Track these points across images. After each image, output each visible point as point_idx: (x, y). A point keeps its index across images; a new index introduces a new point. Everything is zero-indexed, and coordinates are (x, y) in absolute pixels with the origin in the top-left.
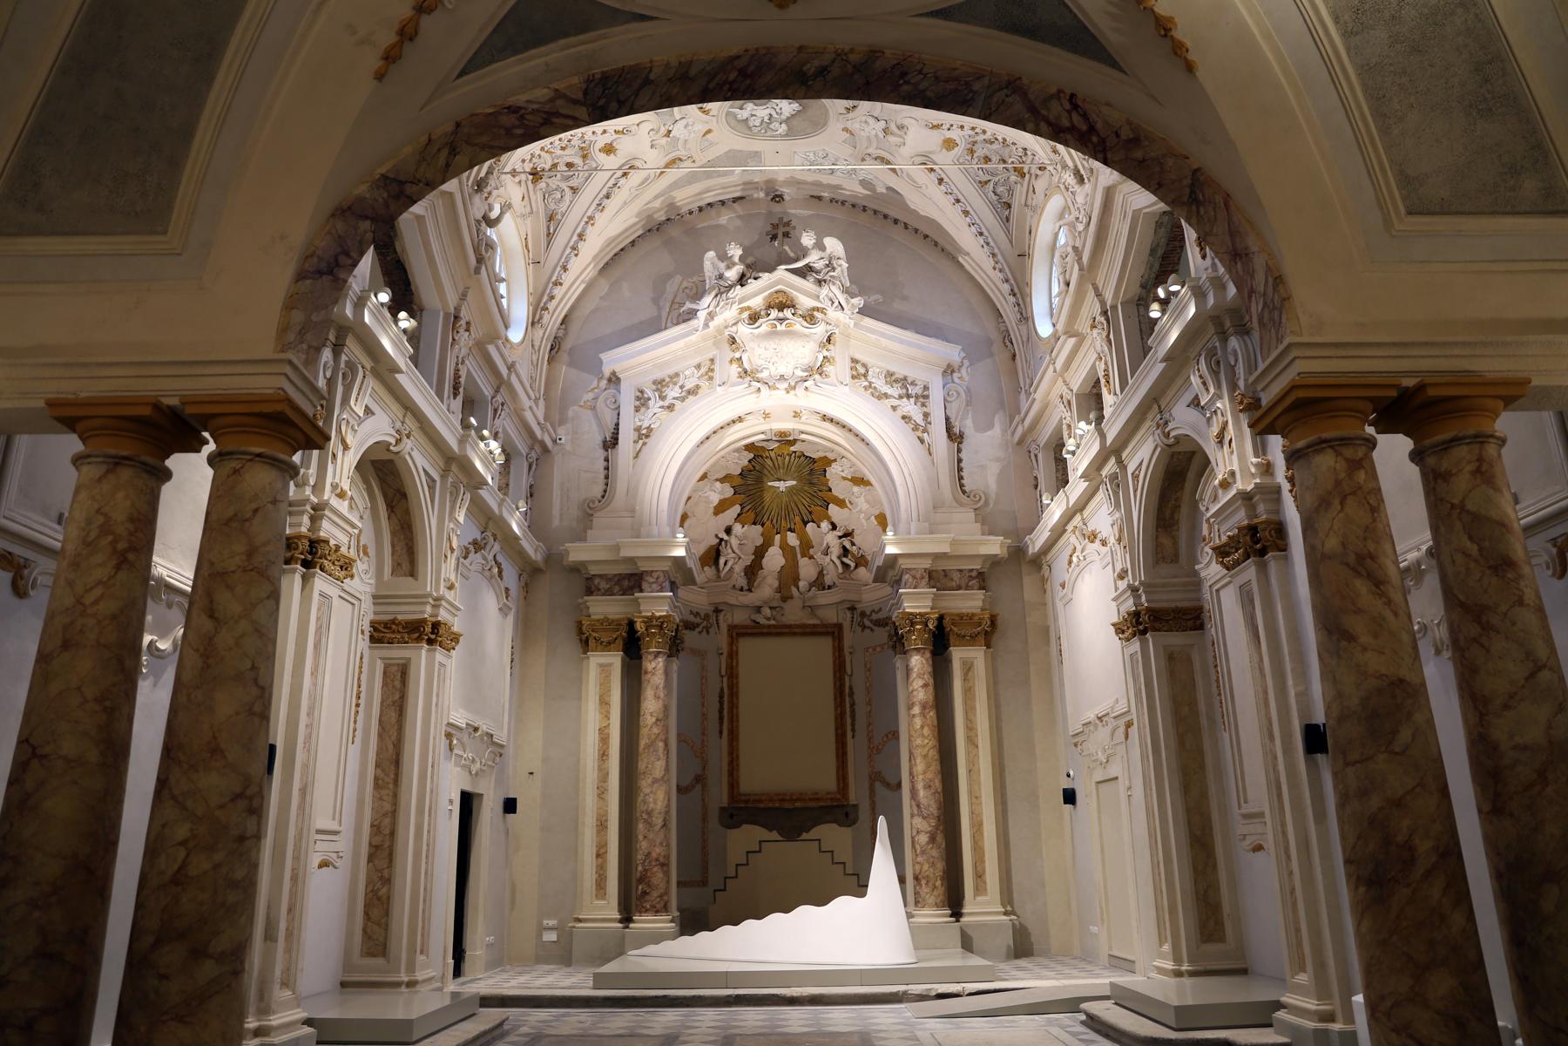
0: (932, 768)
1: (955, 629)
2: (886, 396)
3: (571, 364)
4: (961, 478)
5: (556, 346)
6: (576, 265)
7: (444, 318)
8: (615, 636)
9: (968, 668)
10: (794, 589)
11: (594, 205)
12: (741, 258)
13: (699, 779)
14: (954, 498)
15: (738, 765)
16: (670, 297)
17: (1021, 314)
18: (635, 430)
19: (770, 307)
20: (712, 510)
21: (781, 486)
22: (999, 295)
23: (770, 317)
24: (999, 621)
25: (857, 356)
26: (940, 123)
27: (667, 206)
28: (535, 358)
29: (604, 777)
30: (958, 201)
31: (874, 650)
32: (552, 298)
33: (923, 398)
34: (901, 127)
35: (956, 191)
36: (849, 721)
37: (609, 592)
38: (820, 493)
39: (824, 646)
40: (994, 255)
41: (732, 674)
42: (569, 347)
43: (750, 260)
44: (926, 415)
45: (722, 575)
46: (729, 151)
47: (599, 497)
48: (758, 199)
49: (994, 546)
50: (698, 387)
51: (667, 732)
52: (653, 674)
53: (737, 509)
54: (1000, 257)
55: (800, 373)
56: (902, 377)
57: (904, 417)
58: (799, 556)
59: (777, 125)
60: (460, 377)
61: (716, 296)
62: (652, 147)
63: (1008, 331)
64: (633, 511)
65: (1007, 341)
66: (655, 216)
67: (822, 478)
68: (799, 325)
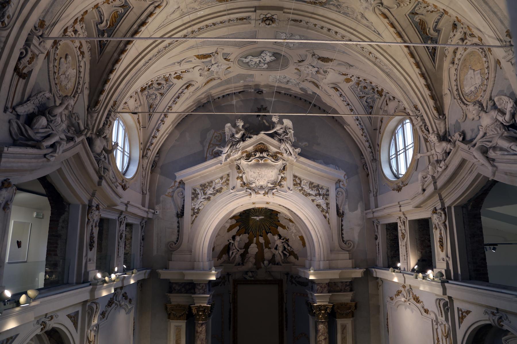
1: (339, 311)
2: (310, 195)
4: (342, 234)
5: (154, 165)
6: (163, 128)
7: (82, 208)
8: (182, 313)
9: (344, 328)
10: (262, 264)
11: (172, 102)
12: (243, 126)
14: (339, 244)
17: (373, 157)
18: (191, 209)
19: (256, 151)
20: (227, 230)
21: (258, 218)
22: (363, 146)
23: (257, 156)
25: (297, 174)
26: (347, 73)
28: (144, 173)
30: (348, 104)
32: (152, 144)
33: (326, 196)
34: (325, 72)
35: (348, 100)
36: (285, 323)
37: (180, 292)
40: (363, 129)
41: (235, 301)
44: (327, 204)
45: (231, 259)
46: (238, 74)
47: (175, 241)
48: (251, 92)
49: (358, 273)
50: (221, 188)
52: (201, 334)
53: (238, 228)
54: (365, 130)
55: (270, 185)
57: (317, 205)
58: (264, 247)
60: (94, 238)
61: (231, 147)
62: (200, 76)
64: (191, 251)
65: (365, 167)
66: (202, 101)
68: (269, 161)
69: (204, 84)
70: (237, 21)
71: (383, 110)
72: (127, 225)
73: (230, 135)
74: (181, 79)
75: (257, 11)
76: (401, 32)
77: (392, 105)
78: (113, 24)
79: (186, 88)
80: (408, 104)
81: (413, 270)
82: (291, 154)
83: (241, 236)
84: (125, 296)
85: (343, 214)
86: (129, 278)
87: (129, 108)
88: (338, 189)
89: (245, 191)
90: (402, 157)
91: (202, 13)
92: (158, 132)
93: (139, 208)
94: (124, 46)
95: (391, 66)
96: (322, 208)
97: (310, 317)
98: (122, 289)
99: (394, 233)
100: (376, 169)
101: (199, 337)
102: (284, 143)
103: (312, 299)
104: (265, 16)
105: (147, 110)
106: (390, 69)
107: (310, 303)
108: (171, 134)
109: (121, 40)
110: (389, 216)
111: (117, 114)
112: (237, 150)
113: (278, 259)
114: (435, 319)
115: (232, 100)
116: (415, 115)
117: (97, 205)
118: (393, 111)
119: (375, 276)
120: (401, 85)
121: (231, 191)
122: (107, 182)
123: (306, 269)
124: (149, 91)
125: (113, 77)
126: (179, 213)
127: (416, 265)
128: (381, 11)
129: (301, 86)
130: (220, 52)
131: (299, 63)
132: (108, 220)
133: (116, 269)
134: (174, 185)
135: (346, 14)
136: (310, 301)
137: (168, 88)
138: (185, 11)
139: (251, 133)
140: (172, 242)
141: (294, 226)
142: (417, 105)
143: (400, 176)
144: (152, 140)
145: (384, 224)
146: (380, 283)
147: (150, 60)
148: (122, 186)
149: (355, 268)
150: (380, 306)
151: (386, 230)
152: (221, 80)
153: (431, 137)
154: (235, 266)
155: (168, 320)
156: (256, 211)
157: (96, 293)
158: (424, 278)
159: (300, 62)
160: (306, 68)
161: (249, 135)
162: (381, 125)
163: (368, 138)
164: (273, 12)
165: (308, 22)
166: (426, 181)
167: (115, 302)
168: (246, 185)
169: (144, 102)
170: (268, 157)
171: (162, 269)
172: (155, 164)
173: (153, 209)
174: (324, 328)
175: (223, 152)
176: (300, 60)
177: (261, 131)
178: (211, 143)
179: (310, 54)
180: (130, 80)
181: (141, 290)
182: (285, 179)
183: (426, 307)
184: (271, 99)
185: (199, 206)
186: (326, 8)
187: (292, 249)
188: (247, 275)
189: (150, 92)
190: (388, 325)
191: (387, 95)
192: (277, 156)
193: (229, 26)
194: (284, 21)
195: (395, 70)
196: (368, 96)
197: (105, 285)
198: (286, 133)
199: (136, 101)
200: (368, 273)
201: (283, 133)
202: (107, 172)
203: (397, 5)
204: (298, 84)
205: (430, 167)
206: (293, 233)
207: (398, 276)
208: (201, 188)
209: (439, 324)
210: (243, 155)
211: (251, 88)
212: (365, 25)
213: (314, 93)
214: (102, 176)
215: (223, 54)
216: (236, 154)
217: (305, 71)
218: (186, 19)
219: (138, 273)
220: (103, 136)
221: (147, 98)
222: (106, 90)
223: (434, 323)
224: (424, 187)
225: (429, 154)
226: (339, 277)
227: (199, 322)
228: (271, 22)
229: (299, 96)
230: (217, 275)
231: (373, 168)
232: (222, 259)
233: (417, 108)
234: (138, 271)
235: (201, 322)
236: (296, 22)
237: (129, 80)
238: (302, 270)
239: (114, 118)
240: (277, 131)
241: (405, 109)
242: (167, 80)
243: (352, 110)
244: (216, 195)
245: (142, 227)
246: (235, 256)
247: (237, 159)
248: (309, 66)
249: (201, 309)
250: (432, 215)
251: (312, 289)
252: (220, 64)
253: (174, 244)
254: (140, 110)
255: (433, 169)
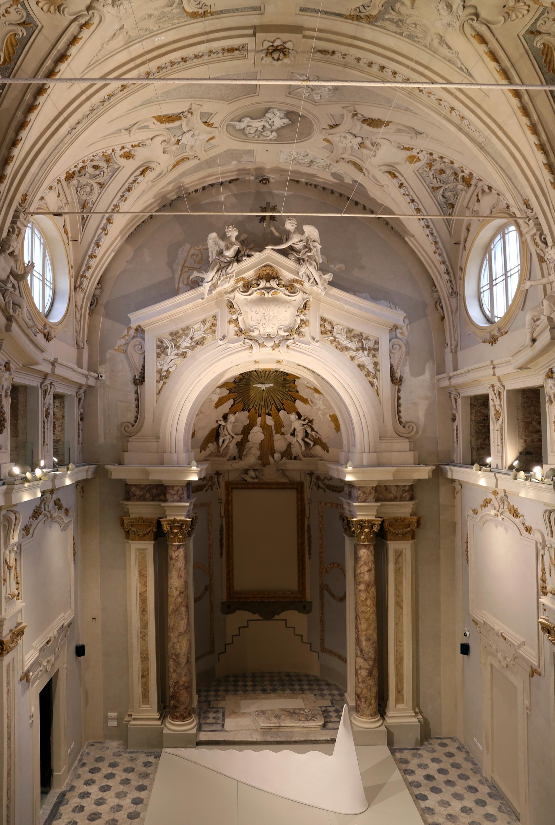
0: (372, 627)
1: (392, 530)
3: (107, 316)
4: (399, 412)
5: (94, 302)
6: (106, 242)
9: (399, 554)
10: (271, 459)
12: (237, 238)
13: (208, 588)
15: (233, 574)
16: (182, 263)
17: (452, 289)
19: (259, 278)
21: (263, 387)
23: (260, 286)
24: (422, 522)
25: (326, 316)
26: (411, 147)
27: (178, 188)
28: (78, 316)
29: (144, 625)
30: (413, 201)
31: (326, 504)
32: (89, 268)
33: (374, 351)
35: (412, 193)
36: (307, 548)
37: (142, 498)
38: (290, 393)
39: (291, 496)
40: (436, 243)
41: (228, 515)
42: (105, 302)
43: (244, 237)
44: (376, 364)
45: (221, 450)
46: (228, 150)
47: (132, 421)
48: (249, 181)
50: (204, 338)
51: (188, 599)
52: (177, 560)
53: (231, 402)
54: (440, 244)
55: (282, 333)
56: (359, 333)
57: (359, 366)
58: (274, 432)
59: (269, 133)
61: (218, 271)
62: (164, 152)
63: (440, 299)
64: (158, 437)
65: (438, 305)
66: (168, 196)
67: (292, 384)
68: (282, 294)
69: (171, 167)
70: (223, 53)
71: (471, 210)
72: (56, 397)
73: (215, 252)
74: (131, 158)
75: (257, 34)
76: (509, 69)
77: (487, 201)
78: (10, 59)
79: (141, 174)
80: (514, 198)
81: (511, 468)
82: (317, 284)
83: (237, 414)
84: (58, 504)
85: (401, 380)
86: (63, 476)
87: (47, 207)
88: (393, 340)
89: (242, 343)
90: (499, 290)
91: (163, 38)
92: (98, 247)
93: (73, 370)
94: (33, 99)
95: (488, 132)
96: (366, 370)
97: (347, 539)
98: (53, 493)
99: (482, 411)
100: (457, 309)
101: (174, 565)
102: (305, 265)
103: (350, 511)
104: (271, 44)
105: (78, 209)
106: (486, 138)
107: (347, 518)
108: (119, 253)
109: (30, 82)
110: (476, 382)
111: (30, 216)
112: (228, 277)
113: (297, 450)
114: (541, 541)
115: (219, 194)
116: (525, 216)
117: (7, 363)
118: (489, 212)
119: (449, 476)
120: (504, 166)
121: (220, 343)
122: (20, 326)
123: (341, 465)
124: (79, 178)
125: (19, 152)
126: (137, 377)
127: (516, 460)
128: (475, 30)
129: (334, 170)
130: (196, 111)
131: (330, 129)
132: (25, 388)
133: (42, 463)
134: (128, 333)
135: (411, 37)
136: (347, 514)
137: (111, 173)
138: (133, 33)
139: (251, 249)
140: (128, 422)
141: (322, 399)
142: (529, 200)
143: (496, 320)
144: (88, 261)
145: (466, 397)
146: (458, 488)
147: (78, 123)
148: (45, 335)
149: (419, 465)
150: (456, 523)
151: (471, 407)
152: (199, 159)
153: (550, 252)
154: (228, 460)
155: (125, 540)
156: (260, 375)
157: (13, 496)
158: (527, 479)
159: (332, 127)
160: (342, 139)
161: (247, 252)
162: (468, 236)
163: (444, 258)
164: (285, 36)
165: (346, 55)
166: (538, 326)
167: (44, 512)
168: (243, 332)
169: (72, 199)
170: (279, 288)
171: (113, 464)
172: (96, 300)
173: (96, 372)
174: (368, 555)
175: (206, 280)
176: (332, 125)
177: (267, 245)
178: (186, 265)
179: (350, 112)
180: (47, 159)
181: (82, 497)
182: (307, 323)
183: (527, 524)
184: (283, 192)
185: (169, 366)
186: (378, 26)
187: (318, 436)
188: (247, 474)
189: (81, 181)
190: (467, 552)
191: (480, 184)
192: (293, 287)
193: (211, 63)
194: (303, 52)
195: (494, 139)
196: (447, 186)
197: (27, 484)
198: (307, 247)
199: (59, 196)
200: (439, 473)
201: (304, 249)
202: (20, 310)
203: (504, 17)
204: (329, 166)
205: (546, 302)
206: (320, 410)
207: (486, 477)
208: (171, 338)
209: (546, 548)
210: (238, 285)
211: (249, 174)
212: (444, 58)
213: (355, 182)
214: (12, 316)
215: (201, 113)
216: (226, 282)
217: (340, 144)
218: (137, 49)
219: (77, 470)
220: (8, 252)
221: (77, 191)
222: (8, 176)
223: (540, 547)
224: (535, 336)
225: (544, 281)
226: (393, 477)
227: (174, 544)
228: (282, 55)
229: (331, 188)
230: (199, 473)
231: (451, 306)
232: (207, 450)
233: (530, 205)
234: (76, 467)
235: (177, 544)
236: (325, 54)
237: (46, 159)
238: (334, 467)
239: (25, 222)
240: (293, 245)
241: (508, 207)
242: (108, 160)
243: (418, 210)
244: (196, 349)
245: (80, 400)
246: (228, 446)
247: (229, 291)
248: (347, 135)
249: (176, 525)
250: (546, 380)
251: (350, 496)
252: (196, 133)
253: (131, 426)
254: (66, 210)
255: (550, 306)
